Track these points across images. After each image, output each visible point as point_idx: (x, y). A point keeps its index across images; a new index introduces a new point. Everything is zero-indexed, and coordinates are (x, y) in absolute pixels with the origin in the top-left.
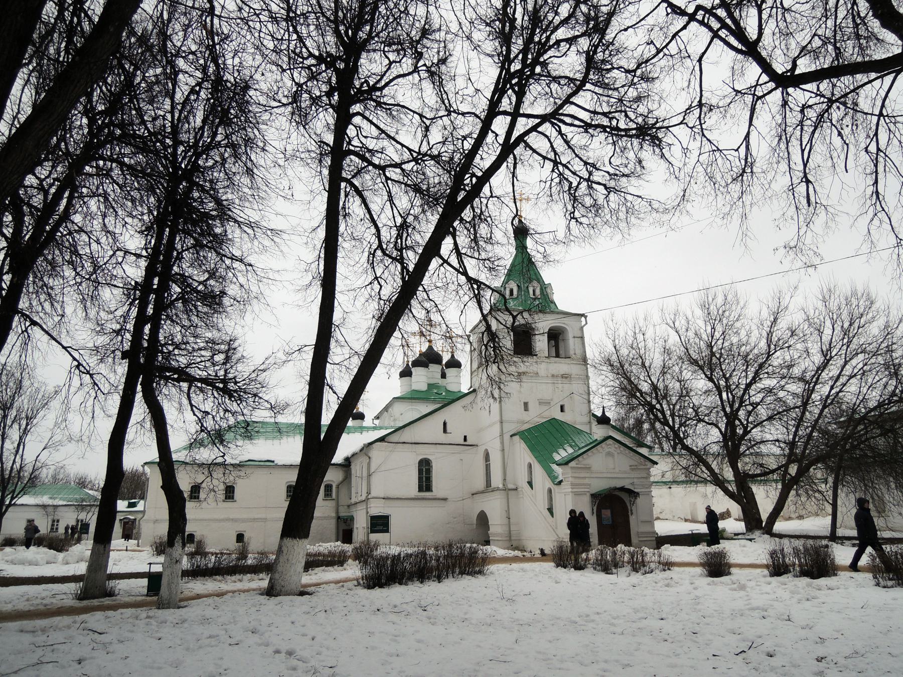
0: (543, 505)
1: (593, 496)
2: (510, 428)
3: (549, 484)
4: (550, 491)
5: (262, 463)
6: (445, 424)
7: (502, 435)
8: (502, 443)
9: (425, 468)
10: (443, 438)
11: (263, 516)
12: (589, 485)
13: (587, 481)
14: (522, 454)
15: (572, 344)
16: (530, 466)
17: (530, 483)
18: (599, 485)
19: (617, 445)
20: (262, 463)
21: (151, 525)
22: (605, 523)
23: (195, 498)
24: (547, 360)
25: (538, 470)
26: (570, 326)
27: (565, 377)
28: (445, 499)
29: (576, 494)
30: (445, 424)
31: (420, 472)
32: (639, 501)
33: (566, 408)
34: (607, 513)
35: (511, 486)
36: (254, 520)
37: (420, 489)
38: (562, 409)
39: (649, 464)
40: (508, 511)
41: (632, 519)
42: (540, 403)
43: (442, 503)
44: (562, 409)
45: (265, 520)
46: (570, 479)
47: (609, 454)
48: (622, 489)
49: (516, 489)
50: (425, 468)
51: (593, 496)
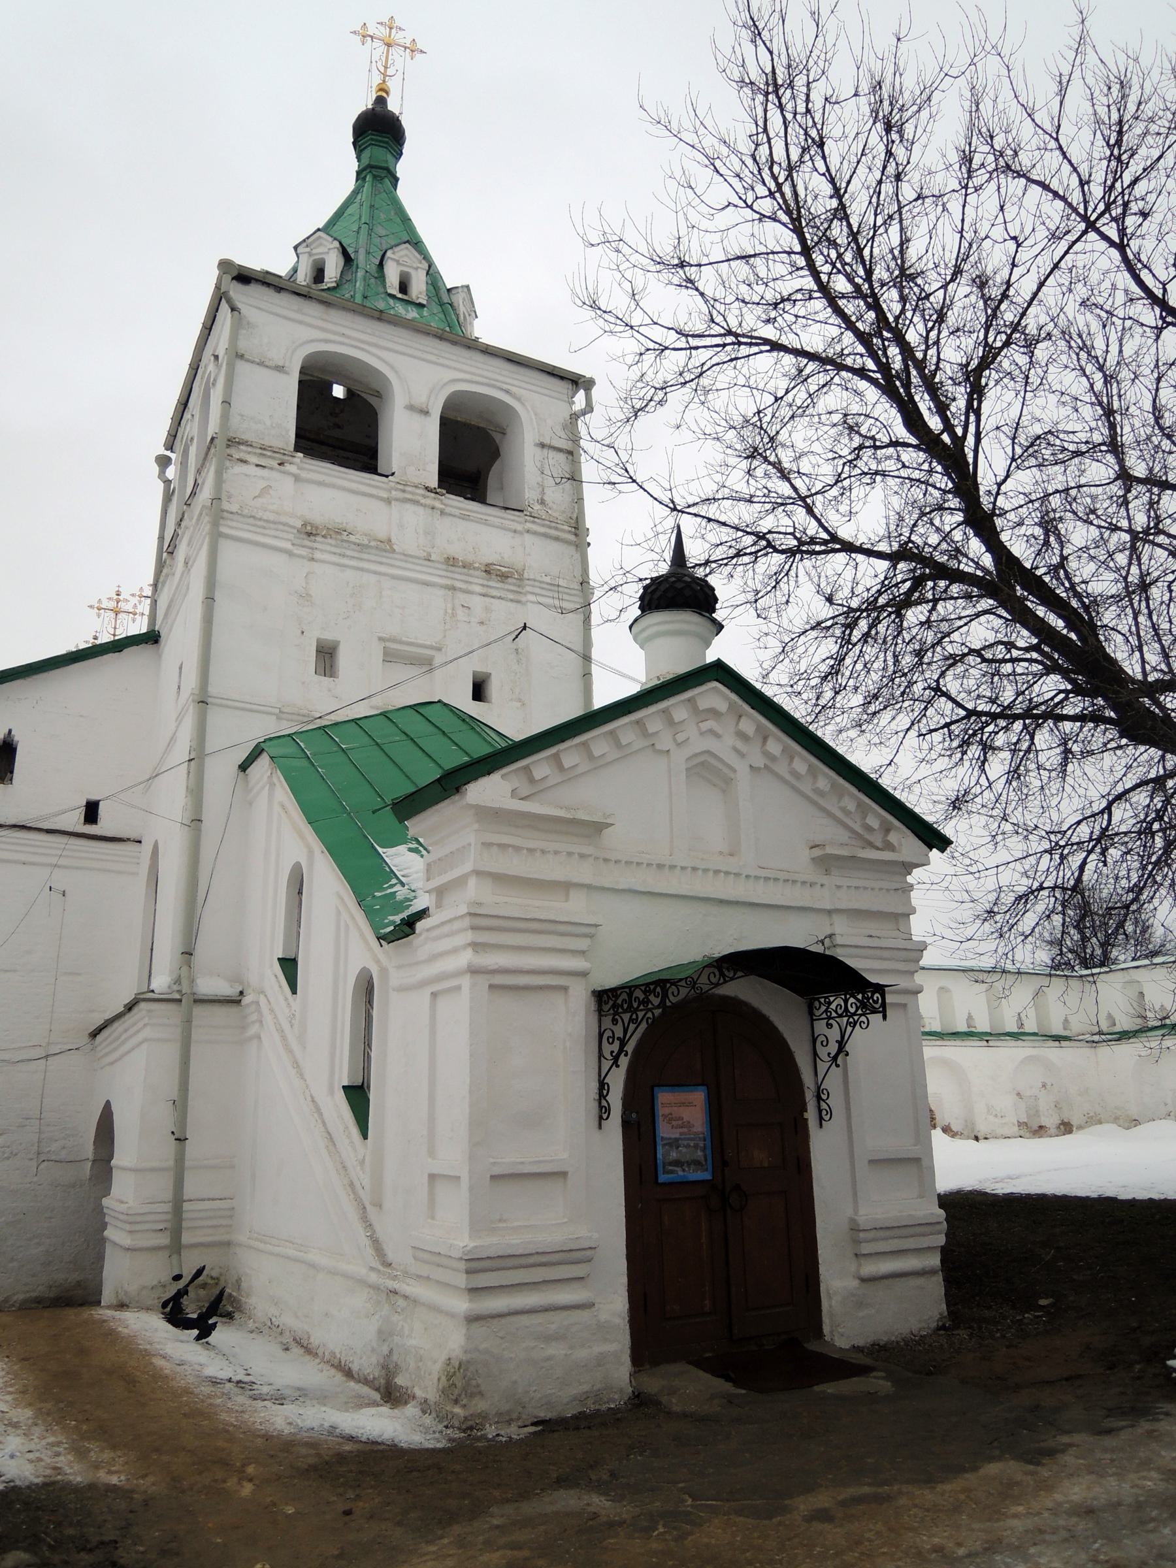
0: (330, 1071)
1: (608, 1001)
2: (236, 733)
3: (363, 950)
4: (366, 990)
7: (198, 758)
8: (196, 792)
12: (590, 931)
13: (576, 908)
14: (277, 833)
15: (528, 465)
16: (297, 884)
17: (289, 966)
19: (752, 721)
24: (431, 499)
25: (328, 886)
26: (534, 414)
27: (498, 574)
29: (503, 986)
34: (684, 1113)
35: (208, 985)
38: (479, 692)
39: (907, 844)
40: (181, 1105)
41: (825, 1149)
42: (390, 657)
44: (479, 692)
46: (473, 889)
47: (707, 770)
49: (235, 1001)
51: (608, 1001)
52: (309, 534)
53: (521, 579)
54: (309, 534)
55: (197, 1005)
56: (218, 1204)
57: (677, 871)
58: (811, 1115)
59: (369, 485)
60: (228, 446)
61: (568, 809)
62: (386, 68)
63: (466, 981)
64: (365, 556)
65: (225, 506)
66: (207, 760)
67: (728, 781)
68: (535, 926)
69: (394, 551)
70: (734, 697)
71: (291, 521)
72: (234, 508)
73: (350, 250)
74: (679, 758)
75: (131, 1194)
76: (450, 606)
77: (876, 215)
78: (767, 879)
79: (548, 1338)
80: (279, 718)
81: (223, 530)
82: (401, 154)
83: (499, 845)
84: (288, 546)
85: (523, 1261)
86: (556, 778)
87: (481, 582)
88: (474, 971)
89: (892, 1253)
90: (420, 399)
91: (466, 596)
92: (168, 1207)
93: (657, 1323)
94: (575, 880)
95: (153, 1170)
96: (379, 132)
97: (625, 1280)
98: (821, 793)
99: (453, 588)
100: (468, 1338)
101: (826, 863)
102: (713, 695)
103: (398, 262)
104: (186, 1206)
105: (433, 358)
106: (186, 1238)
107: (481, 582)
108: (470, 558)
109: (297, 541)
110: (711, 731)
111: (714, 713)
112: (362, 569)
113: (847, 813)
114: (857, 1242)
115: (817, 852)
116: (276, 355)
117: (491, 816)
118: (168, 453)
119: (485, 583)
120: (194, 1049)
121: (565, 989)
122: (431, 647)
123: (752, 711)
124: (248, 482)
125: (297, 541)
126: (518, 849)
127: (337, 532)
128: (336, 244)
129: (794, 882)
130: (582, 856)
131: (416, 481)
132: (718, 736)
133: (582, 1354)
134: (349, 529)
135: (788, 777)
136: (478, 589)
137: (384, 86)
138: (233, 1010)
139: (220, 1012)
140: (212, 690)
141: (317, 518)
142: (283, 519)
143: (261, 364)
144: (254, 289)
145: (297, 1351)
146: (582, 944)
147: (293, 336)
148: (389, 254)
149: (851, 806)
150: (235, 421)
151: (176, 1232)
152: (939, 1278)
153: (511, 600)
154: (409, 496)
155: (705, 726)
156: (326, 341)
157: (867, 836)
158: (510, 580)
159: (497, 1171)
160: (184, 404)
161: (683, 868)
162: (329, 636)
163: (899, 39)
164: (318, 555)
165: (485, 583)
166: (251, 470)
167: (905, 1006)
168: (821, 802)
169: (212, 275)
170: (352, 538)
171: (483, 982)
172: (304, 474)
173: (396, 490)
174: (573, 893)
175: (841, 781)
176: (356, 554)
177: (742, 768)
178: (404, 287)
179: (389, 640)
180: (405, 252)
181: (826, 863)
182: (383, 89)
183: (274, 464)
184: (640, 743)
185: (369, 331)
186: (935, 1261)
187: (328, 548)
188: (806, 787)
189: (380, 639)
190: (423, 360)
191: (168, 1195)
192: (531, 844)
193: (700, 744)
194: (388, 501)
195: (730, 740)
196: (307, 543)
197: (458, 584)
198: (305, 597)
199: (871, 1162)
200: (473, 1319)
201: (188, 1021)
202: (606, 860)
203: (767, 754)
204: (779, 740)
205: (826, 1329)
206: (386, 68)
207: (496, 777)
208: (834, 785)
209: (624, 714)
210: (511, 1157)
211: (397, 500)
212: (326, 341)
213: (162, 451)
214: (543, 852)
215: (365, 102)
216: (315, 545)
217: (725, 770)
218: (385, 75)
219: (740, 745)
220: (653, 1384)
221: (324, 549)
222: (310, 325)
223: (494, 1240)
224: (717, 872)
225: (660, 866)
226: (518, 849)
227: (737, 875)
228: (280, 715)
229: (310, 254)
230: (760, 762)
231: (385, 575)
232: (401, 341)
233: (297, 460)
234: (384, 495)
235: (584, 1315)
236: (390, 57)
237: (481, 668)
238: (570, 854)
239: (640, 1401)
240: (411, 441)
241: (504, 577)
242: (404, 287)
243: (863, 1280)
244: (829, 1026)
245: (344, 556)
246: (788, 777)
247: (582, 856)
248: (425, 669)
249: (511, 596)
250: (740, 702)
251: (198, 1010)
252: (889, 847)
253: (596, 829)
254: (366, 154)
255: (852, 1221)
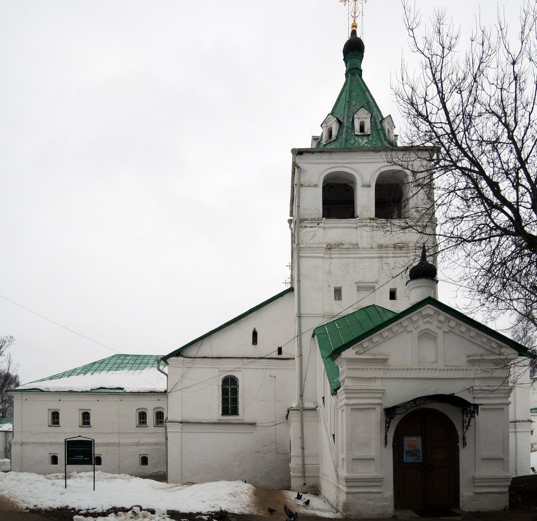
5: (112, 391)
6: (255, 334)
9: (230, 389)
10: (250, 350)
11: (116, 441)
12: (383, 392)
13: (378, 385)
18: (400, 393)
20: (112, 391)
21: (19, 447)
22: (407, 459)
23: (144, 422)
28: (253, 424)
30: (255, 334)
31: (225, 392)
32: (482, 418)
33: (398, 295)
35: (307, 405)
36: (108, 444)
37: (225, 412)
41: (465, 457)
42: (359, 289)
43: (250, 429)
44: (393, 295)
45: (119, 445)
47: (426, 335)
48: (451, 400)
49: (314, 409)
50: (230, 389)
51: (390, 413)
52: (329, 249)
53: (408, 247)
54: (329, 249)
55: (305, 411)
56: (315, 466)
57: (414, 370)
58: (460, 444)
59: (349, 223)
60: (300, 223)
61: (373, 355)
62: (355, 13)
63: (344, 408)
64: (349, 252)
65: (301, 246)
66: (302, 335)
67: (436, 338)
68: (364, 391)
69: (359, 248)
70: (436, 308)
71: (322, 246)
72: (304, 246)
73: (340, 119)
74: (416, 333)
75: (295, 463)
76: (380, 264)
77: (464, 124)
78: (448, 370)
79: (369, 500)
80: (323, 318)
81: (302, 255)
82: (363, 56)
83: (353, 369)
84: (322, 255)
85: (361, 480)
86: (381, 341)
87: (392, 252)
88: (346, 405)
89: (487, 486)
90: (367, 180)
91: (387, 259)
92: (301, 466)
93: (401, 498)
94: (377, 376)
95: (297, 456)
96: (354, 49)
97: (392, 487)
98: (472, 337)
99: (382, 257)
100: (347, 497)
101: (472, 362)
102: (429, 309)
103: (359, 118)
104: (306, 466)
105: (372, 160)
106: (307, 474)
107: (392, 252)
108: (388, 243)
109: (325, 252)
110: (428, 322)
111: (429, 315)
112: (348, 258)
113: (484, 343)
114: (474, 482)
115: (469, 359)
116: (314, 181)
117: (350, 360)
118: (292, 218)
119: (394, 252)
120: (304, 423)
121: (375, 408)
122: (374, 282)
123: (443, 313)
124: (309, 234)
125: (325, 252)
126: (359, 369)
127: (339, 245)
128: (335, 119)
129: (459, 370)
130: (380, 369)
131: (366, 217)
132: (430, 323)
133: (378, 504)
134: (343, 243)
135: (459, 333)
136: (391, 255)
137: (355, 24)
138: (315, 412)
139: (311, 412)
140: (302, 312)
141: (332, 242)
142: (320, 245)
143: (309, 186)
144: (305, 156)
145: (327, 502)
146: (380, 395)
147: (318, 170)
148: (355, 116)
149: (485, 340)
150: (302, 212)
151: (304, 472)
152: (508, 495)
153: (405, 257)
154: (364, 224)
155: (425, 320)
156: (331, 168)
157: (492, 350)
158: (404, 249)
159: (354, 458)
160: (292, 200)
161: (416, 369)
162: (338, 285)
163: (472, 40)
164: (333, 256)
165: (394, 252)
166: (309, 229)
167: (503, 409)
168: (473, 340)
169: (289, 158)
170: (344, 247)
171: (349, 408)
172: (326, 226)
173: (359, 222)
174: (377, 381)
175: (480, 332)
176: (346, 252)
177: (440, 333)
178: (362, 129)
179: (359, 283)
180: (362, 112)
181: (472, 362)
182: (354, 26)
183: (316, 224)
184: (401, 330)
185: (347, 157)
186: (506, 490)
187: (336, 252)
188: (466, 336)
189: (356, 283)
190: (368, 163)
191: (301, 463)
192: (363, 367)
193: (423, 327)
194: (356, 228)
195: (436, 323)
196: (329, 252)
197: (384, 255)
198: (330, 273)
199: (482, 459)
200: (348, 493)
201: (302, 416)
202: (388, 369)
203: (449, 326)
204: (454, 321)
205: (461, 506)
206: (355, 13)
207: (351, 349)
208: (477, 334)
209: (408, 314)
210: (358, 454)
211: (360, 227)
212: (331, 168)
213: (289, 218)
214: (367, 369)
215: (346, 37)
216: (332, 252)
217: (434, 334)
218: (355, 17)
219: (439, 325)
220: (398, 513)
221: (335, 253)
222: (325, 163)
223: (353, 475)
224: (428, 369)
225: (407, 369)
226: (359, 369)
227: (436, 369)
228: (324, 316)
229: (327, 126)
230: (447, 329)
231: (356, 258)
232: (359, 157)
233: (323, 221)
234: (355, 226)
235: (380, 495)
236: (357, 6)
237: (392, 287)
238: (375, 369)
239: (394, 517)
240: (365, 200)
241: (401, 248)
242: (362, 129)
243: (475, 493)
244: (467, 417)
245: (341, 254)
246: (459, 333)
247: (380, 369)
248: (372, 291)
249: (404, 255)
250: (438, 310)
251: (305, 413)
252: (501, 354)
253: (385, 361)
254: (349, 63)
255: (473, 476)
